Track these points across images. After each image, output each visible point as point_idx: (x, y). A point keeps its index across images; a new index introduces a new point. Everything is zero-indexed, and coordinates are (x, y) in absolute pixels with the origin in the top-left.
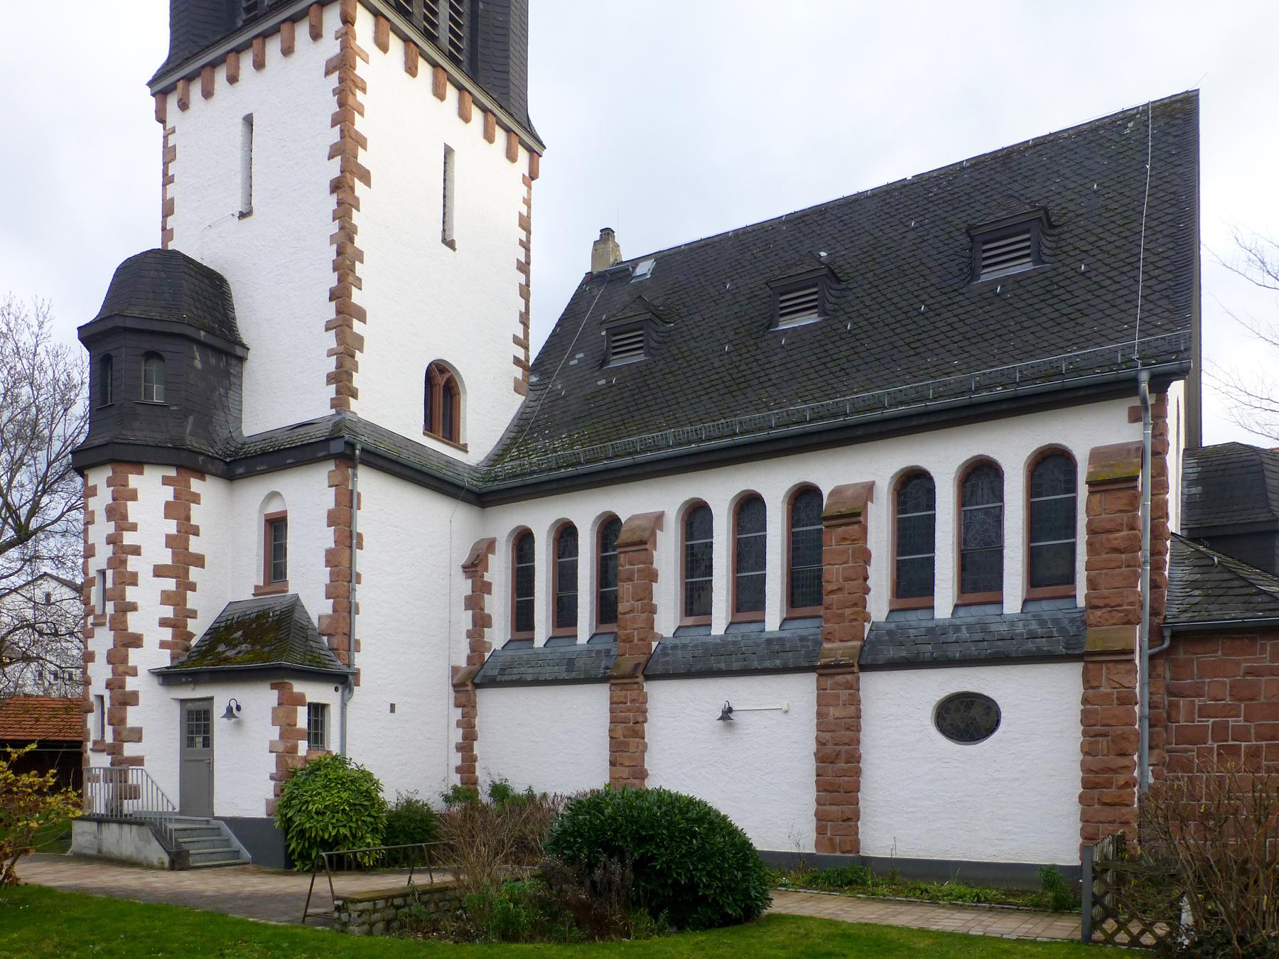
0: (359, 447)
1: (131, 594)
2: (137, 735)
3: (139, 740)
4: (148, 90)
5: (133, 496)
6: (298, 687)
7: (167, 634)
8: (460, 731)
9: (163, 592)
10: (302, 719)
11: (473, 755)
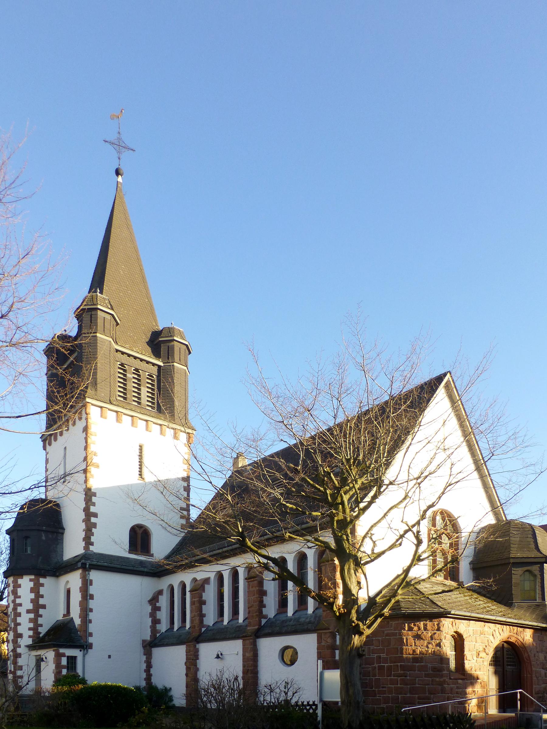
0: (88, 564)
1: (19, 620)
5: (20, 586)
6: (62, 651)
7: (31, 633)
8: (145, 664)
9: (30, 618)
10: (64, 661)
11: (150, 674)
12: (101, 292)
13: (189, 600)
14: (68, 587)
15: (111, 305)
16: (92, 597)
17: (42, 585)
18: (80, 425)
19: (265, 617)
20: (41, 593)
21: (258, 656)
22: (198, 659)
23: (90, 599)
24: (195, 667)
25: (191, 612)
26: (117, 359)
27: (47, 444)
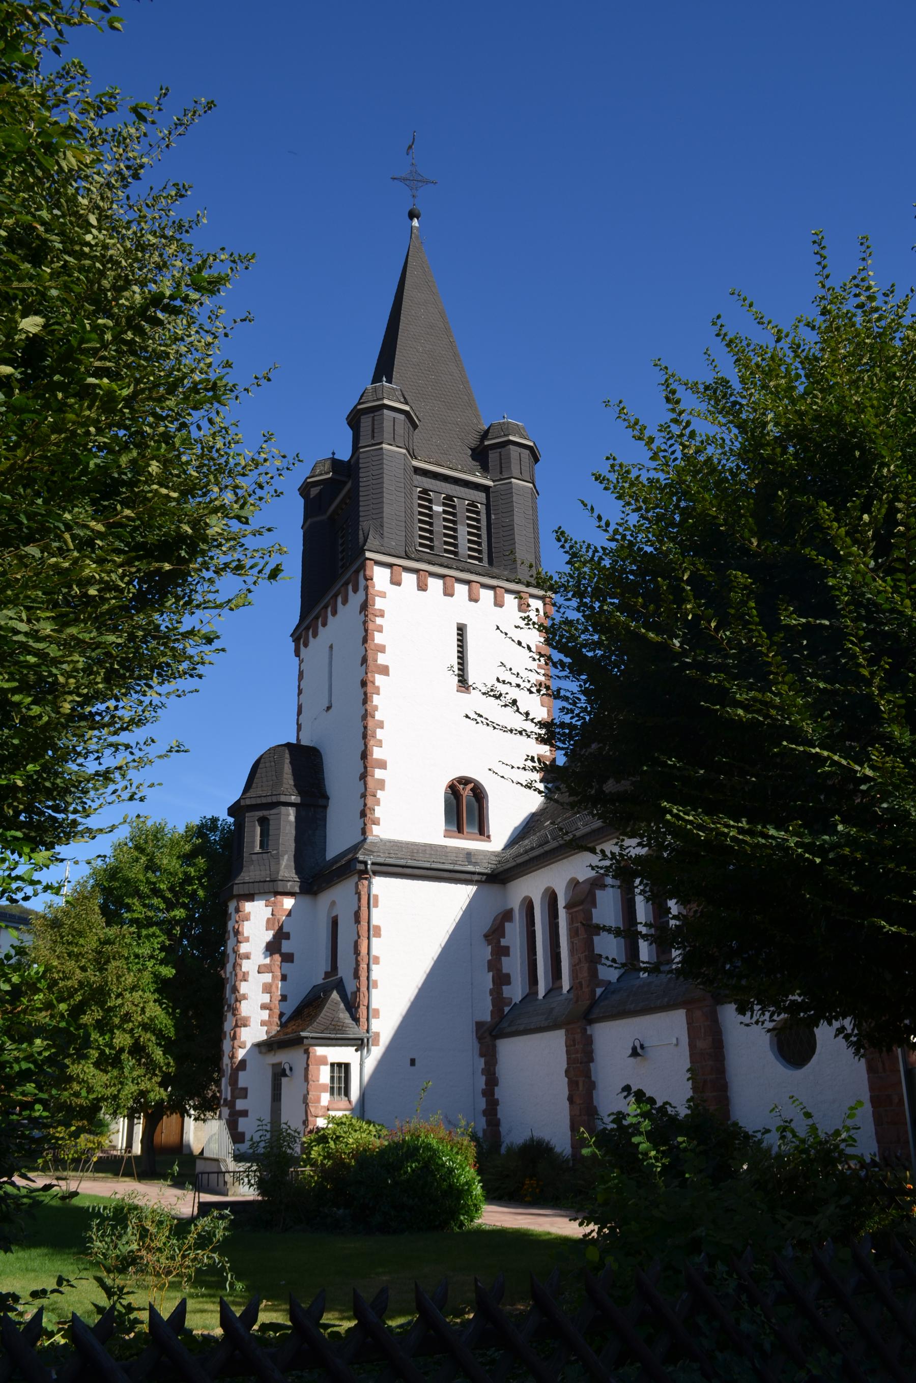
0: (369, 862)
2: (244, 1093)
3: (245, 1097)
4: (291, 639)
7: (265, 1014)
8: (484, 1078)
12: (389, 381)
13: (566, 938)
14: (334, 914)
15: (404, 398)
18: (355, 600)
21: (723, 1047)
22: (591, 1060)
23: (374, 936)
25: (572, 951)
26: (416, 483)
27: (302, 646)
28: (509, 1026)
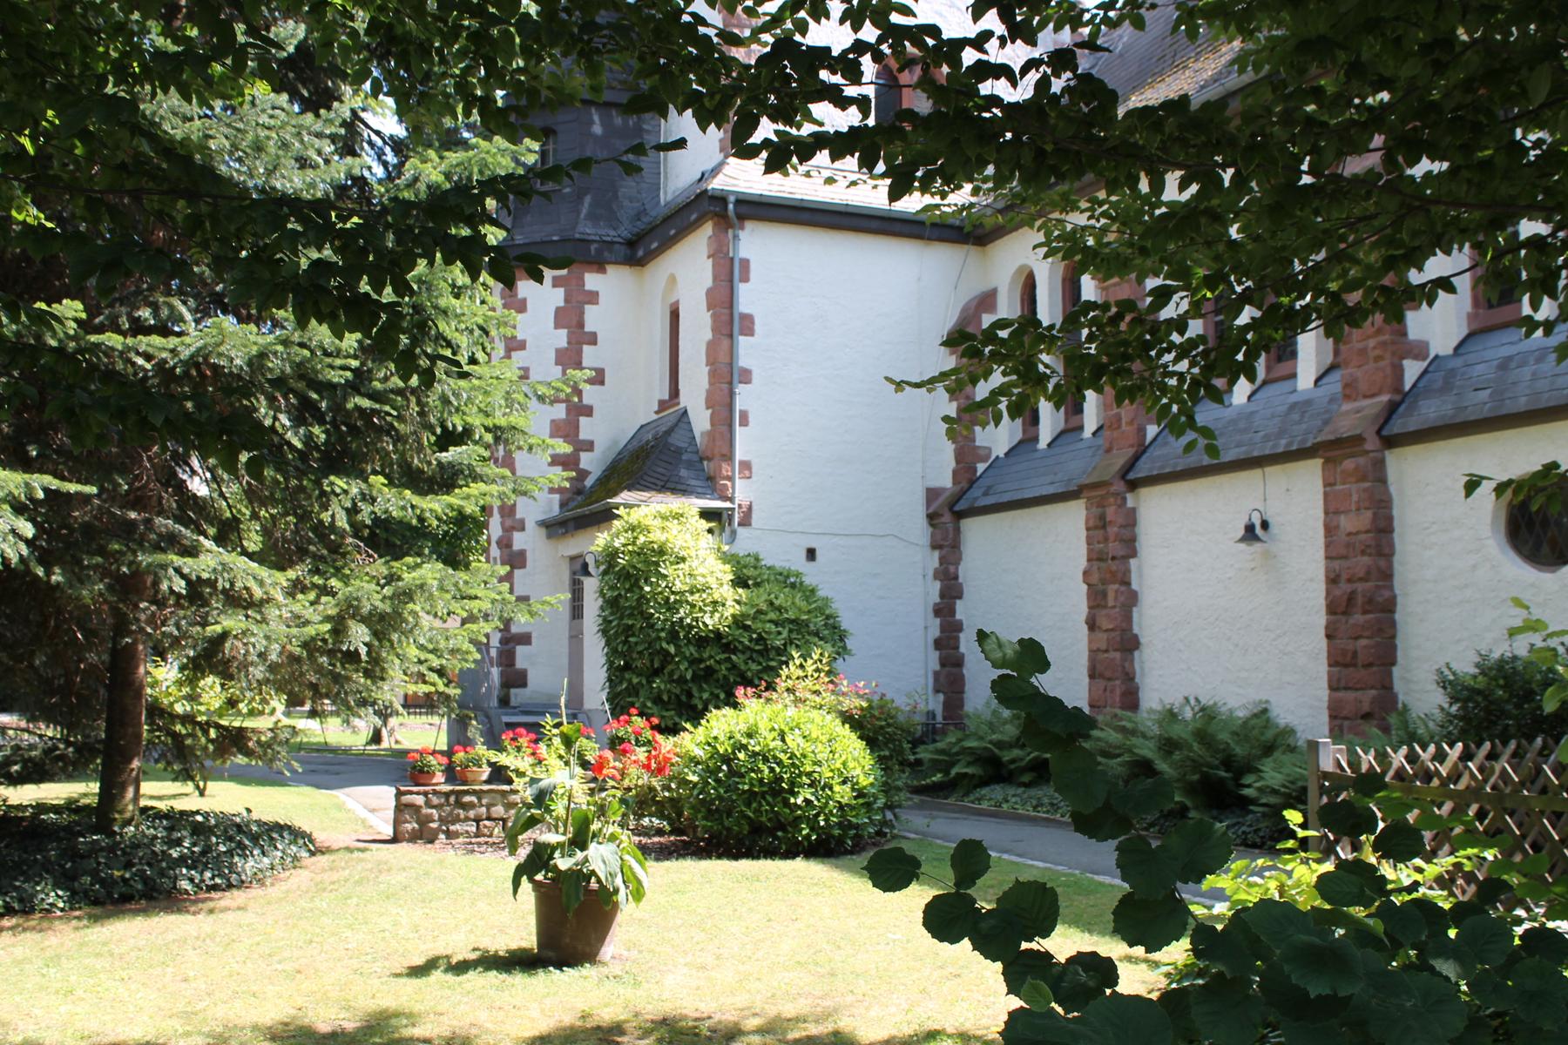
8: (938, 585)
9: (553, 421)
16: (748, 325)
17: (593, 297)
19: (1420, 351)
20: (588, 328)
24: (1123, 588)
28: (986, 494)
